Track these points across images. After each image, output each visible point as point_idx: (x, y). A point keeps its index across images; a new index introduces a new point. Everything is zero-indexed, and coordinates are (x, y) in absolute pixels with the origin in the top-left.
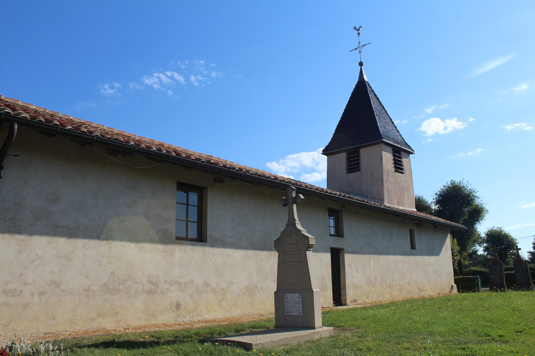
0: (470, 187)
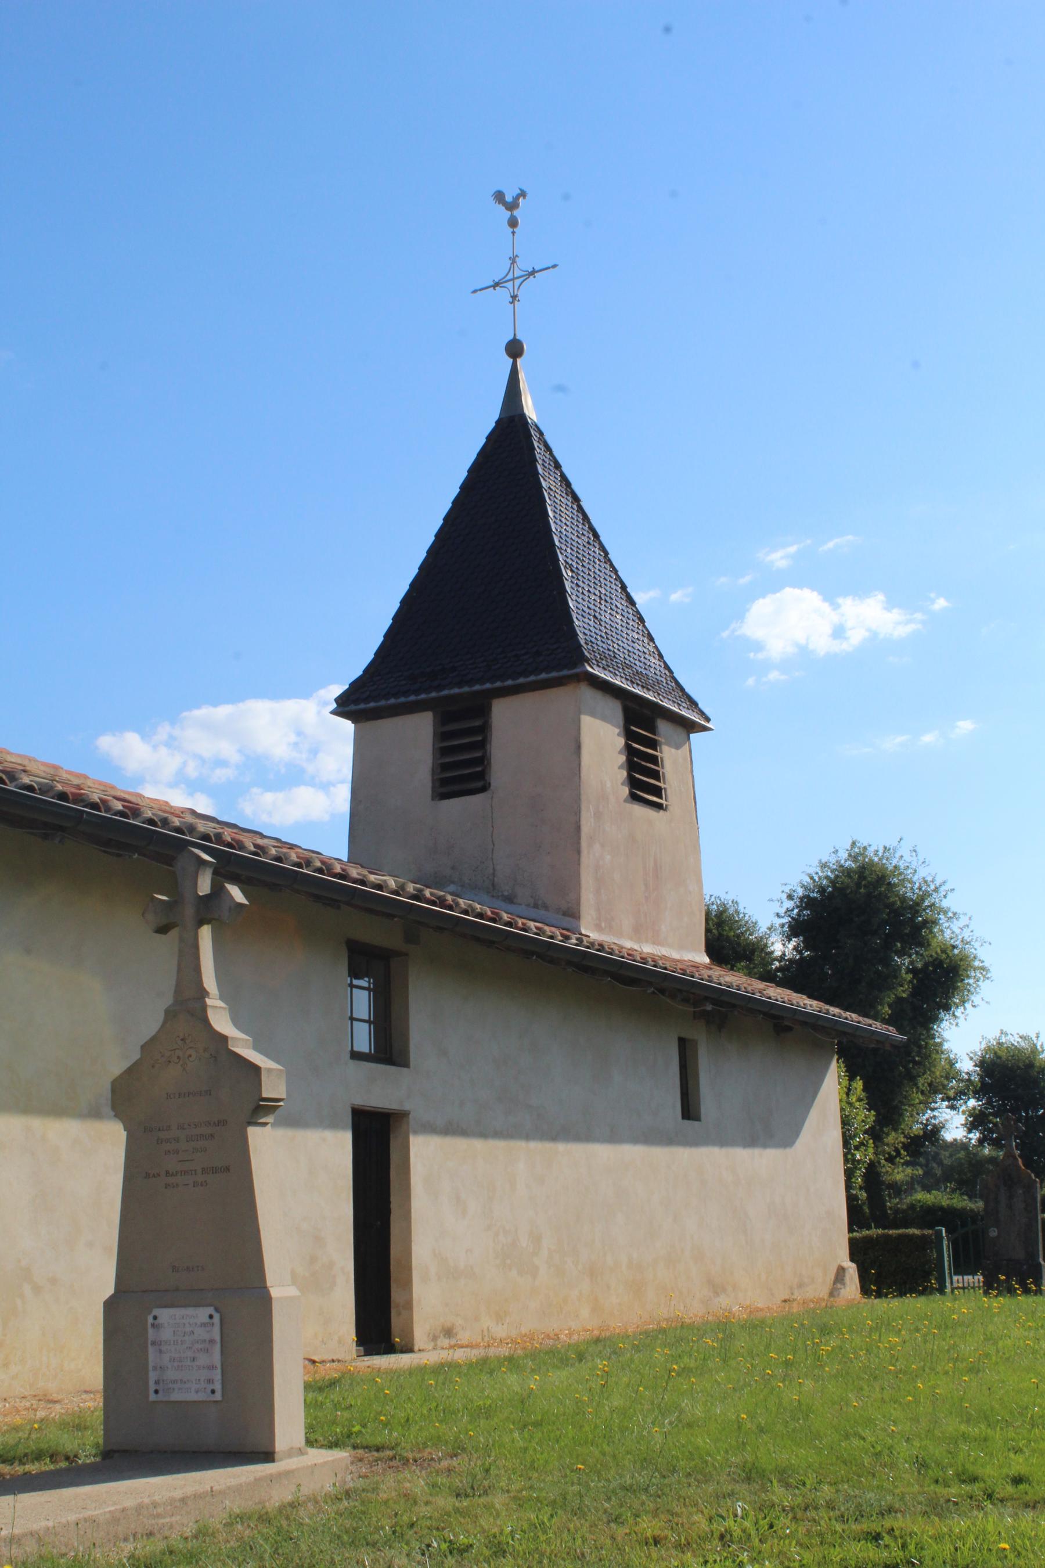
0: (923, 873)
